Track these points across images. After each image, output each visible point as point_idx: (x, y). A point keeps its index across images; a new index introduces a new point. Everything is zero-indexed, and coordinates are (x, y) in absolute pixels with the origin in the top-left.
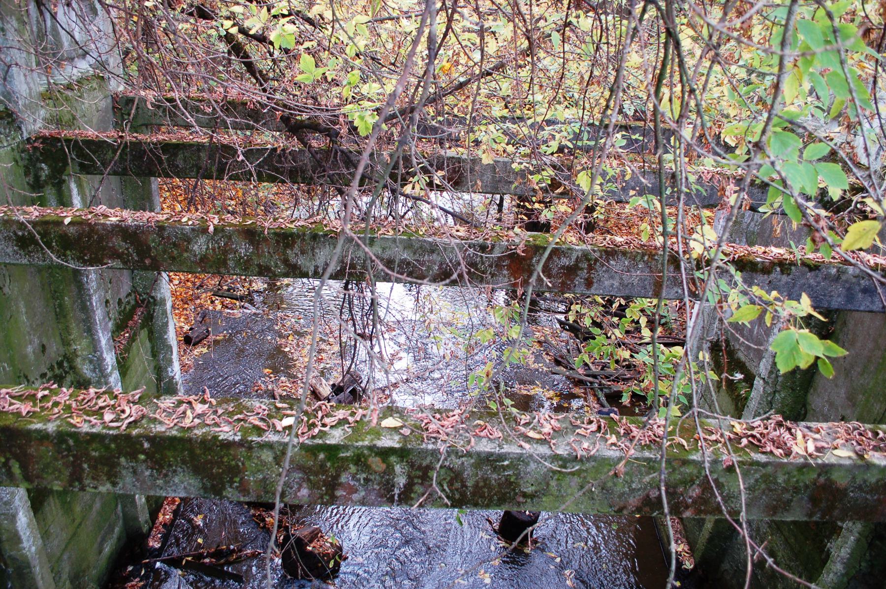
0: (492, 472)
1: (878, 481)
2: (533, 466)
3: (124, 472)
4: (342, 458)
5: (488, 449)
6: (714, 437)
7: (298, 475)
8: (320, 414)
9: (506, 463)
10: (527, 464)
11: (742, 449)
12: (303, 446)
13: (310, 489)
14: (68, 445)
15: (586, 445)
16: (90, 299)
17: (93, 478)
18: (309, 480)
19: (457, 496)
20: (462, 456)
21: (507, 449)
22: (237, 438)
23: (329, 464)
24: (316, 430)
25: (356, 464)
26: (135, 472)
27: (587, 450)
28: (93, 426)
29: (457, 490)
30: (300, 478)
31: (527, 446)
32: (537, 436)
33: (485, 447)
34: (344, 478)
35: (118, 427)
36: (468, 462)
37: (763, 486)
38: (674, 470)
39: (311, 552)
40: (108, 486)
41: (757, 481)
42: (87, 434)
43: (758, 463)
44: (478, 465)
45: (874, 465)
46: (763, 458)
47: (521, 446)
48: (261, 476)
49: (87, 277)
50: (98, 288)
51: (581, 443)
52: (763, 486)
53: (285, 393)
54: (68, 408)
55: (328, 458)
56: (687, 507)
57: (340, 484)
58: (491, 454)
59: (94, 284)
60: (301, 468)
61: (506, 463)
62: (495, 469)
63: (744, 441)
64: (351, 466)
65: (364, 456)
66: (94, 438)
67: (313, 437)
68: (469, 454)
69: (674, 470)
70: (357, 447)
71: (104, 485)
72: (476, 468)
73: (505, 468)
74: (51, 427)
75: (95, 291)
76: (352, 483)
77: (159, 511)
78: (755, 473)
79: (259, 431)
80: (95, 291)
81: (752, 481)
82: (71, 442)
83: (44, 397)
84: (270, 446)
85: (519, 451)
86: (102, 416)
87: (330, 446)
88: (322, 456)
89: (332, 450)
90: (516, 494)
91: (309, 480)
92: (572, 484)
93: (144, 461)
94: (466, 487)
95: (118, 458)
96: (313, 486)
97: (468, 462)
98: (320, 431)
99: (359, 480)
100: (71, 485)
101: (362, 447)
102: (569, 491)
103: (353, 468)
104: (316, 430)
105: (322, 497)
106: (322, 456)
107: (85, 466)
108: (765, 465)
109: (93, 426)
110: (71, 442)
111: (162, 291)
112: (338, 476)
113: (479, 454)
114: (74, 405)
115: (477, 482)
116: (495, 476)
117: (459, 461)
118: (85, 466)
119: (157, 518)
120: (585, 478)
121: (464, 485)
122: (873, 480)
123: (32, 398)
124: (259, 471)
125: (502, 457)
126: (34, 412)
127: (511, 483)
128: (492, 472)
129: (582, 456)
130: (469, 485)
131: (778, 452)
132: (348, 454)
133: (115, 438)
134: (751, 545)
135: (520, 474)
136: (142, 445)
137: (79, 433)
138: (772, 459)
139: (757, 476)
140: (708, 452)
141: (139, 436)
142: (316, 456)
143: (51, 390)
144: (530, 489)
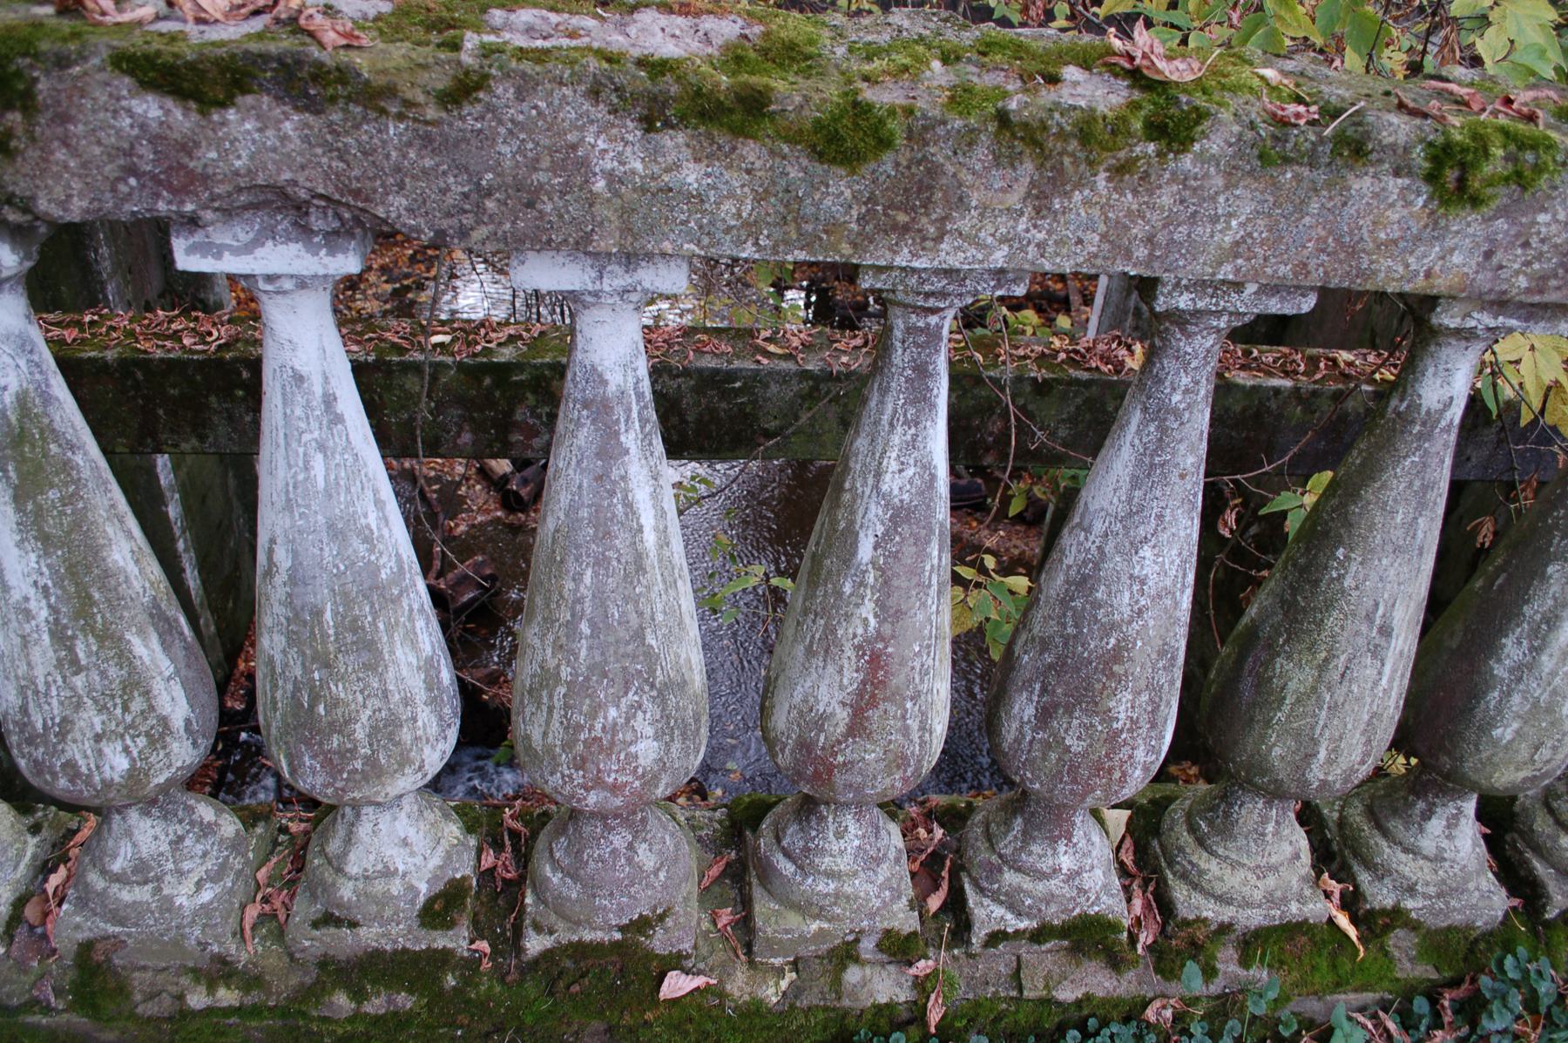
0: (720, 400)
1: (1244, 410)
2: (774, 388)
3: (215, 419)
4: (516, 383)
5: (712, 365)
6: (1021, 352)
7: (456, 412)
8: (483, 331)
9: (738, 385)
10: (766, 386)
11: (1059, 365)
12: (460, 366)
13: (474, 432)
14: (136, 380)
15: (844, 359)
16: (103, 290)
17: (172, 431)
18: (472, 419)
19: (675, 438)
20: (678, 376)
21: (737, 364)
22: (371, 359)
23: (497, 394)
24: (479, 348)
25: (535, 392)
26: (230, 418)
27: (847, 365)
28: (169, 351)
29: (674, 427)
30: (460, 416)
31: (765, 361)
32: (779, 351)
33: (709, 362)
34: (520, 414)
35: (204, 352)
36: (686, 384)
37: (1088, 416)
38: (965, 391)
39: (486, 702)
40: (194, 442)
41: (1078, 408)
42: (162, 360)
43: (1077, 381)
44: (698, 390)
45: (1237, 386)
46: (1085, 376)
47: (758, 362)
48: (406, 416)
49: (96, 252)
50: (114, 272)
51: (838, 358)
52: (1088, 416)
53: (433, 474)
54: (131, 334)
55: (497, 384)
56: (987, 450)
57: (515, 424)
58: (716, 372)
59: (107, 264)
60: (460, 401)
61: (738, 385)
62: (726, 395)
63: (1062, 356)
64: (529, 395)
65: (545, 377)
66: (170, 365)
67: (475, 355)
68: (687, 373)
69: (965, 391)
70: (535, 366)
71: (187, 441)
72: (698, 394)
73: (737, 392)
74: (110, 355)
75: (111, 276)
76: (531, 421)
77: (238, 656)
78: (1075, 396)
79: (401, 350)
80: (111, 276)
81: (1072, 409)
82: (140, 376)
83: (92, 323)
84: (416, 368)
85: (753, 366)
86: (180, 340)
87: (498, 364)
88: (487, 381)
89: (502, 371)
90: (754, 432)
91: (472, 419)
92: (830, 415)
93: (244, 399)
94: (686, 422)
95: (207, 397)
96: (478, 428)
97: (686, 384)
98: (485, 348)
99: (539, 417)
100: (141, 444)
101: (542, 365)
102: (826, 427)
103: (531, 398)
104: (479, 348)
105: (491, 446)
106: (487, 381)
107: (161, 412)
108: (1088, 384)
109: (169, 351)
110: (140, 376)
111: (217, 289)
112: (511, 412)
113: (700, 371)
114: (138, 329)
115: (701, 415)
116: (724, 405)
117: (674, 384)
118: (161, 412)
119: (235, 665)
120: (845, 405)
121: (683, 421)
122: (1238, 408)
123: (79, 324)
124: (403, 407)
125: (731, 376)
126: (83, 340)
127: (746, 415)
128: (720, 400)
129: (839, 372)
130: (689, 419)
131: (1105, 369)
132: (523, 377)
133: (201, 365)
134: (1017, 418)
135: (756, 401)
136: (240, 374)
137: (151, 360)
138: (1096, 376)
139: (1079, 401)
140: (1010, 367)
141: (235, 360)
142: (480, 382)
143: (101, 316)
144: (772, 425)
